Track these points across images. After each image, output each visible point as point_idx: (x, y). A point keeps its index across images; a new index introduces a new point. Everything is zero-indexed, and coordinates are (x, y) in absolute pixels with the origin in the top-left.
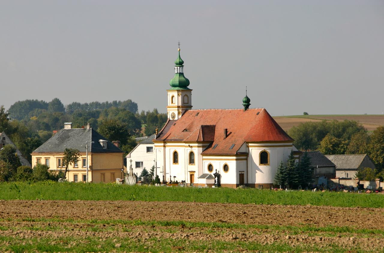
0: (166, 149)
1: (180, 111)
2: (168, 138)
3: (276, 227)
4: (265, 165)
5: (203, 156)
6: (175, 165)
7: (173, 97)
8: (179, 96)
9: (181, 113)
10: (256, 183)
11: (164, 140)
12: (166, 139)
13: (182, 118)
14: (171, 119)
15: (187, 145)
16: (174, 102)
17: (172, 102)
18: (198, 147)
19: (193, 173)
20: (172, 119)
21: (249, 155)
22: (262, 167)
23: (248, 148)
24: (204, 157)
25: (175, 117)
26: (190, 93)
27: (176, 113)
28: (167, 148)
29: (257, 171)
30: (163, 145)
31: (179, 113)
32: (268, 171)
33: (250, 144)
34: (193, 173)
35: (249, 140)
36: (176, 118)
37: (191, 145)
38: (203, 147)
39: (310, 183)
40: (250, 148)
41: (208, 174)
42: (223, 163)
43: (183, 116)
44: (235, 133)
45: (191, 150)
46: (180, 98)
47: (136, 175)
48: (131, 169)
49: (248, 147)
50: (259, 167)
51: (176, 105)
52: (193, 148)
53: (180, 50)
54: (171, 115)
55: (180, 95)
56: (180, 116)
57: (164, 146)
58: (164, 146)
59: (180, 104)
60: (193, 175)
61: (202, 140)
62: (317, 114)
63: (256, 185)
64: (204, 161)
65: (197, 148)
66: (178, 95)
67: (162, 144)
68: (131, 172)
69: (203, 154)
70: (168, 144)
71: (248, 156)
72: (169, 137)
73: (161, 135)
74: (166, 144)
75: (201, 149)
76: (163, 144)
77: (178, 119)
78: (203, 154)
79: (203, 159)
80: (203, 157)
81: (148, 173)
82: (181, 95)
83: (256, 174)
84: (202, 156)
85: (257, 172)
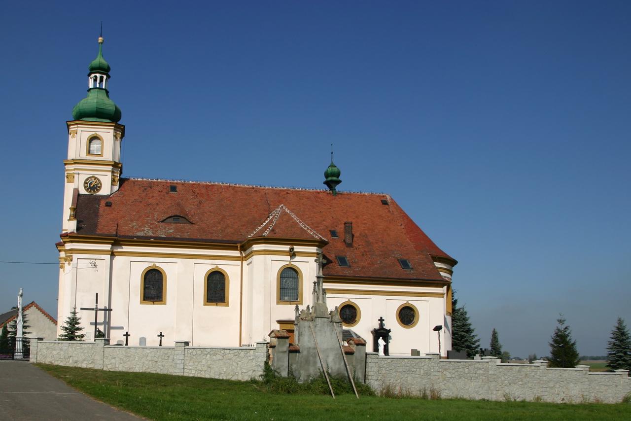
6: (215, 310)
15: (286, 248)
25: (100, 187)
37: (297, 249)
42: (398, 302)
45: (288, 263)
52: (297, 258)
56: (116, 188)
57: (113, 255)
58: (113, 255)
67: (108, 247)
70: (126, 249)
74: (114, 247)
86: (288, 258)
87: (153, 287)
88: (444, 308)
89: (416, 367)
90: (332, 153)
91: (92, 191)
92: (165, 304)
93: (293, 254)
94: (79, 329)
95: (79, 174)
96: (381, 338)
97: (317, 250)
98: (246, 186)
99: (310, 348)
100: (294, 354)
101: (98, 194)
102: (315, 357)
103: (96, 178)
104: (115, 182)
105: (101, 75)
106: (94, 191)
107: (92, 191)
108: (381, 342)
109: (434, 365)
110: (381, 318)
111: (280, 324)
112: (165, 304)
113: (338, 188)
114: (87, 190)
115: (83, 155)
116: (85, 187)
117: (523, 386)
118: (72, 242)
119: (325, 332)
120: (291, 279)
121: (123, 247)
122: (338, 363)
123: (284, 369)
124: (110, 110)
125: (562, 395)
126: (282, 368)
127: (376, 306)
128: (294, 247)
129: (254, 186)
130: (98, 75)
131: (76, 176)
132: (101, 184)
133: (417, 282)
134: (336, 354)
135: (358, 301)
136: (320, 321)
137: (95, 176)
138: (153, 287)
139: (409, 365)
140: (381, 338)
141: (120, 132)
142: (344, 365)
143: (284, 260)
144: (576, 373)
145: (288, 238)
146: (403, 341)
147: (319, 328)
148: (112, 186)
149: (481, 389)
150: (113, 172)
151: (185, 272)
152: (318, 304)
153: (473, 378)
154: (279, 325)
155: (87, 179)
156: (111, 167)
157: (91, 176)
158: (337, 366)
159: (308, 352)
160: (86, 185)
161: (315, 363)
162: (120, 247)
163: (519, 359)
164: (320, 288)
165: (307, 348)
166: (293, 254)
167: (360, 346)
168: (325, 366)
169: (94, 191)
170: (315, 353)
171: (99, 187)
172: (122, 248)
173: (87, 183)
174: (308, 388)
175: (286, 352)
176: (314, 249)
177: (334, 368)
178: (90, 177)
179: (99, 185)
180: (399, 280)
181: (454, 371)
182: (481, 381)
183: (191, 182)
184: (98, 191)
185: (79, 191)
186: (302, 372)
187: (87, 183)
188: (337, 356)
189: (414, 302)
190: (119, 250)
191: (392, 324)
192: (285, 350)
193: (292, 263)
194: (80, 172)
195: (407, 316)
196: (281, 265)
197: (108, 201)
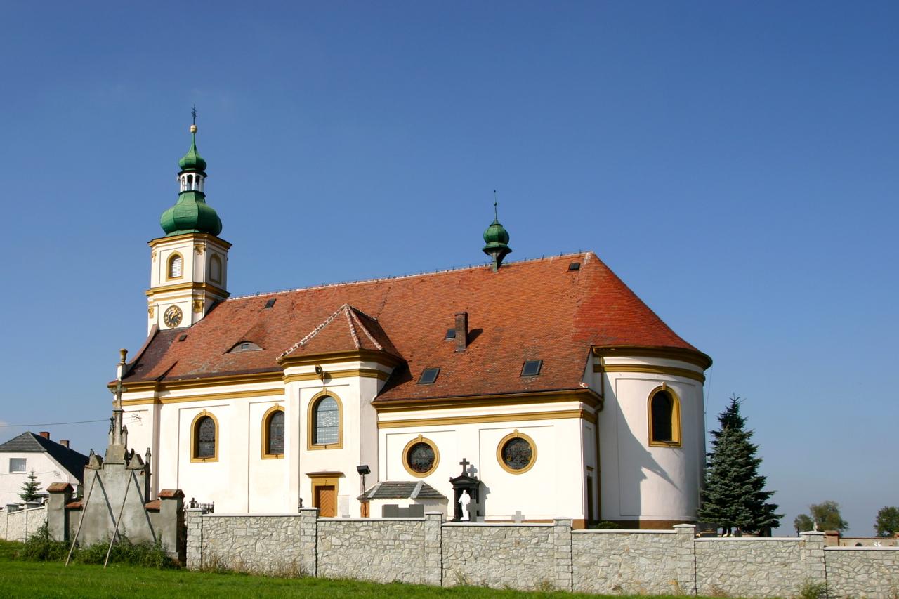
0: (162, 411)
1: (202, 298)
2: (169, 375)
3: (104, 577)
4: (670, 447)
5: (378, 412)
6: (272, 462)
7: (174, 258)
8: (199, 251)
9: (203, 304)
10: (641, 518)
11: (160, 379)
12: (166, 373)
13: (207, 323)
14: (163, 327)
15: (311, 369)
16: (176, 272)
17: (170, 275)
18: (363, 373)
19: (330, 482)
20: (167, 328)
21: (607, 403)
22: (660, 453)
23: (598, 375)
24: (385, 417)
25: (180, 318)
26: (224, 253)
27: (186, 306)
28: (167, 409)
29: (645, 471)
30: (153, 396)
31: (196, 307)
32: (678, 471)
33: (609, 360)
34: (329, 479)
35: (605, 343)
36: (186, 322)
37: (326, 368)
38: (380, 375)
39: (884, 520)
40: (611, 376)
41: (415, 484)
42: (497, 434)
43: (210, 315)
44: (496, 340)
45: (321, 389)
46: (202, 258)
47: (144, 459)
48: (118, 431)
49: (600, 369)
50: (653, 456)
51: (188, 278)
52: (333, 381)
53: (196, 129)
54: (166, 315)
55: (203, 251)
56: (200, 316)
57: (158, 402)
58: (158, 402)
59: (201, 278)
60: (332, 488)
61: (357, 346)
62: (645, 302)
63: (583, 526)
64: (383, 432)
65: (356, 381)
66: (197, 249)
67: (151, 394)
68: (117, 443)
69: (381, 404)
70: (174, 393)
71: (601, 408)
72: (171, 372)
73: (138, 371)
74: (162, 393)
75: (373, 384)
76: (153, 392)
77: (192, 325)
78: (381, 404)
79: (380, 425)
80: (380, 415)
81: (45, 530)
82: (205, 250)
83: (644, 485)
84: (374, 410)
85: (645, 477)
86: (319, 382)
87: (204, 440)
88: (218, 445)
89: (271, 530)
90: (496, 205)
91: (173, 325)
92: (217, 460)
93: (326, 376)
94: (765, 496)
95: (158, 306)
96: (464, 491)
97: (361, 365)
98: (369, 282)
99: (98, 504)
100: (76, 512)
101: (179, 326)
102: (105, 516)
103: (175, 307)
104: (199, 307)
105: (188, 174)
106: (175, 324)
107: (173, 325)
108: (465, 498)
109: (305, 527)
110: (465, 460)
111: (312, 478)
112: (217, 460)
113: (507, 259)
114: (167, 324)
115: (165, 282)
116: (165, 320)
117: (507, 562)
118: (128, 391)
119: (119, 483)
120: (331, 412)
121: (171, 391)
122: (139, 524)
123: (59, 532)
124: (191, 217)
125: (615, 580)
126: (55, 530)
127: (465, 440)
128: (322, 366)
129: (380, 280)
130: (194, 175)
131: (156, 308)
132: (182, 314)
133: (493, 399)
134: (136, 512)
135: (432, 435)
136: (111, 468)
137: (176, 305)
138: (204, 440)
139: (258, 526)
140: (464, 491)
141: (204, 242)
142: (149, 527)
143: (315, 387)
144: (656, 539)
145: (316, 359)
146: (507, 495)
147: (109, 478)
148: (195, 314)
149: (406, 565)
150: (194, 296)
151: (239, 415)
152: (113, 447)
153: (388, 547)
154: (310, 479)
155: (167, 311)
156: (191, 290)
157: (171, 305)
158: (138, 528)
159: (96, 510)
160: (166, 318)
161: (106, 523)
162: (167, 392)
163: (828, 520)
164: (118, 425)
165: (94, 505)
166: (326, 376)
167: (167, 500)
168: (120, 529)
169: (175, 324)
170: (105, 511)
171: (179, 318)
172: (170, 393)
173: (167, 315)
174: (97, 557)
175: (61, 509)
176: (357, 365)
177: (133, 530)
178: (171, 308)
179: (179, 316)
180: (492, 397)
181: (347, 536)
182: (407, 552)
183: (298, 290)
184: (179, 323)
185: (158, 327)
186: (88, 536)
187: (167, 315)
188: (138, 515)
189: (528, 429)
190: (167, 396)
191: (491, 472)
192: (59, 507)
193: (329, 389)
194: (159, 303)
195: (516, 454)
196: (655, 385)
197: (183, 336)
